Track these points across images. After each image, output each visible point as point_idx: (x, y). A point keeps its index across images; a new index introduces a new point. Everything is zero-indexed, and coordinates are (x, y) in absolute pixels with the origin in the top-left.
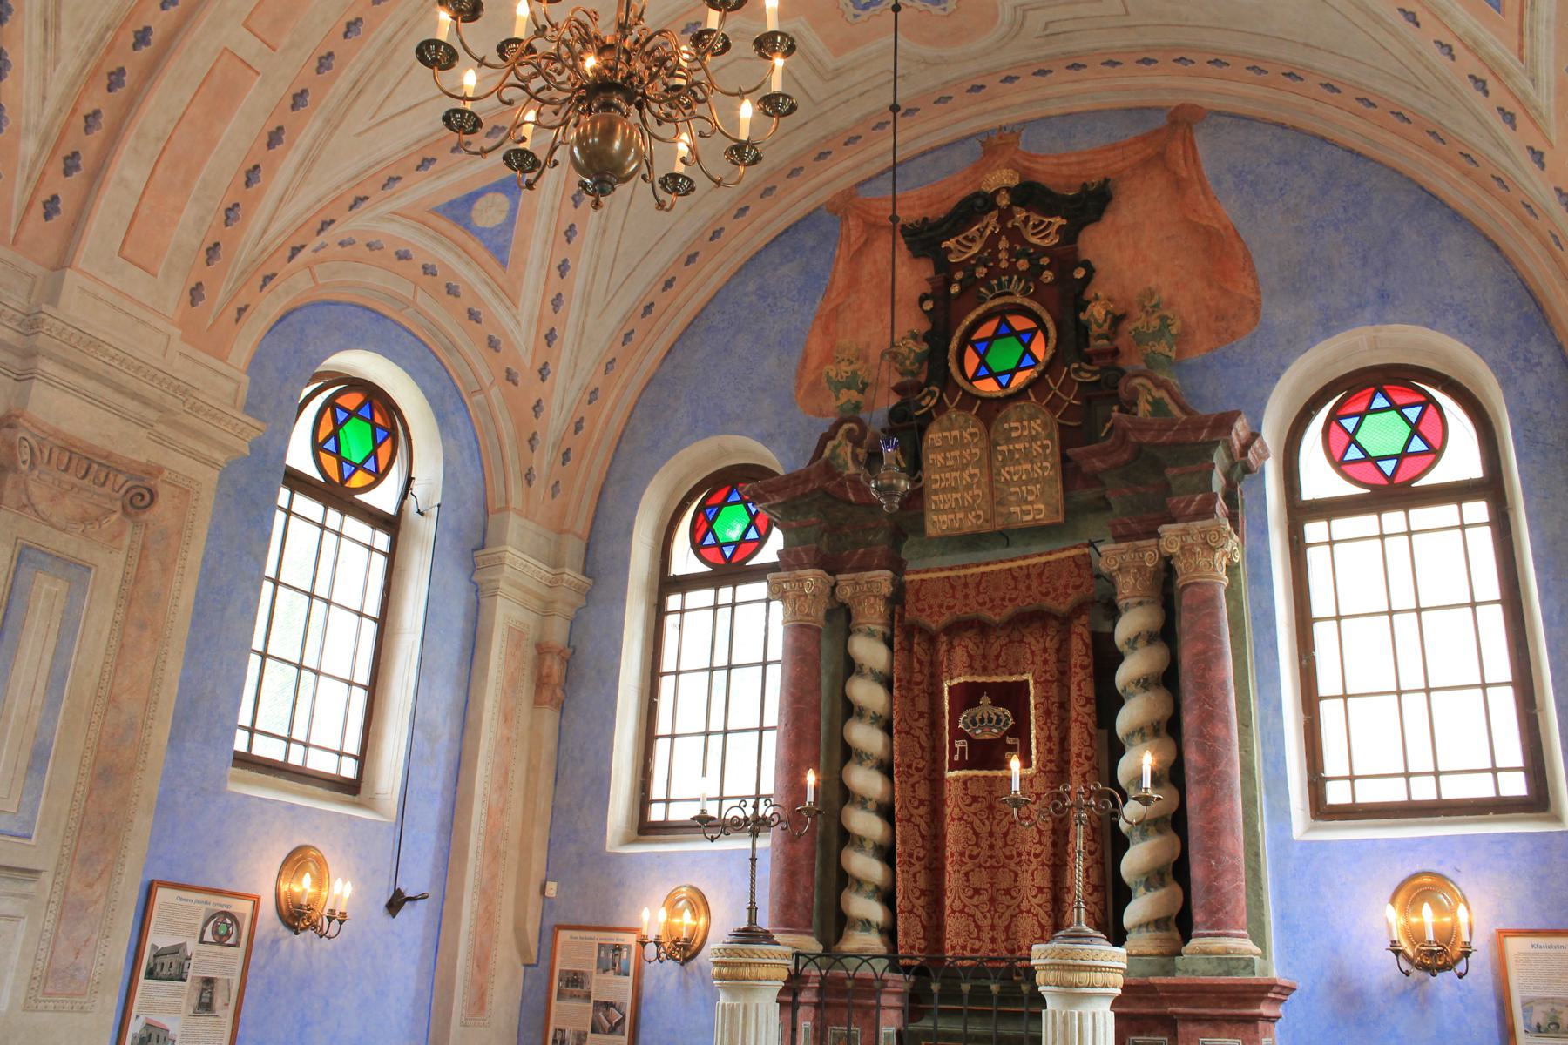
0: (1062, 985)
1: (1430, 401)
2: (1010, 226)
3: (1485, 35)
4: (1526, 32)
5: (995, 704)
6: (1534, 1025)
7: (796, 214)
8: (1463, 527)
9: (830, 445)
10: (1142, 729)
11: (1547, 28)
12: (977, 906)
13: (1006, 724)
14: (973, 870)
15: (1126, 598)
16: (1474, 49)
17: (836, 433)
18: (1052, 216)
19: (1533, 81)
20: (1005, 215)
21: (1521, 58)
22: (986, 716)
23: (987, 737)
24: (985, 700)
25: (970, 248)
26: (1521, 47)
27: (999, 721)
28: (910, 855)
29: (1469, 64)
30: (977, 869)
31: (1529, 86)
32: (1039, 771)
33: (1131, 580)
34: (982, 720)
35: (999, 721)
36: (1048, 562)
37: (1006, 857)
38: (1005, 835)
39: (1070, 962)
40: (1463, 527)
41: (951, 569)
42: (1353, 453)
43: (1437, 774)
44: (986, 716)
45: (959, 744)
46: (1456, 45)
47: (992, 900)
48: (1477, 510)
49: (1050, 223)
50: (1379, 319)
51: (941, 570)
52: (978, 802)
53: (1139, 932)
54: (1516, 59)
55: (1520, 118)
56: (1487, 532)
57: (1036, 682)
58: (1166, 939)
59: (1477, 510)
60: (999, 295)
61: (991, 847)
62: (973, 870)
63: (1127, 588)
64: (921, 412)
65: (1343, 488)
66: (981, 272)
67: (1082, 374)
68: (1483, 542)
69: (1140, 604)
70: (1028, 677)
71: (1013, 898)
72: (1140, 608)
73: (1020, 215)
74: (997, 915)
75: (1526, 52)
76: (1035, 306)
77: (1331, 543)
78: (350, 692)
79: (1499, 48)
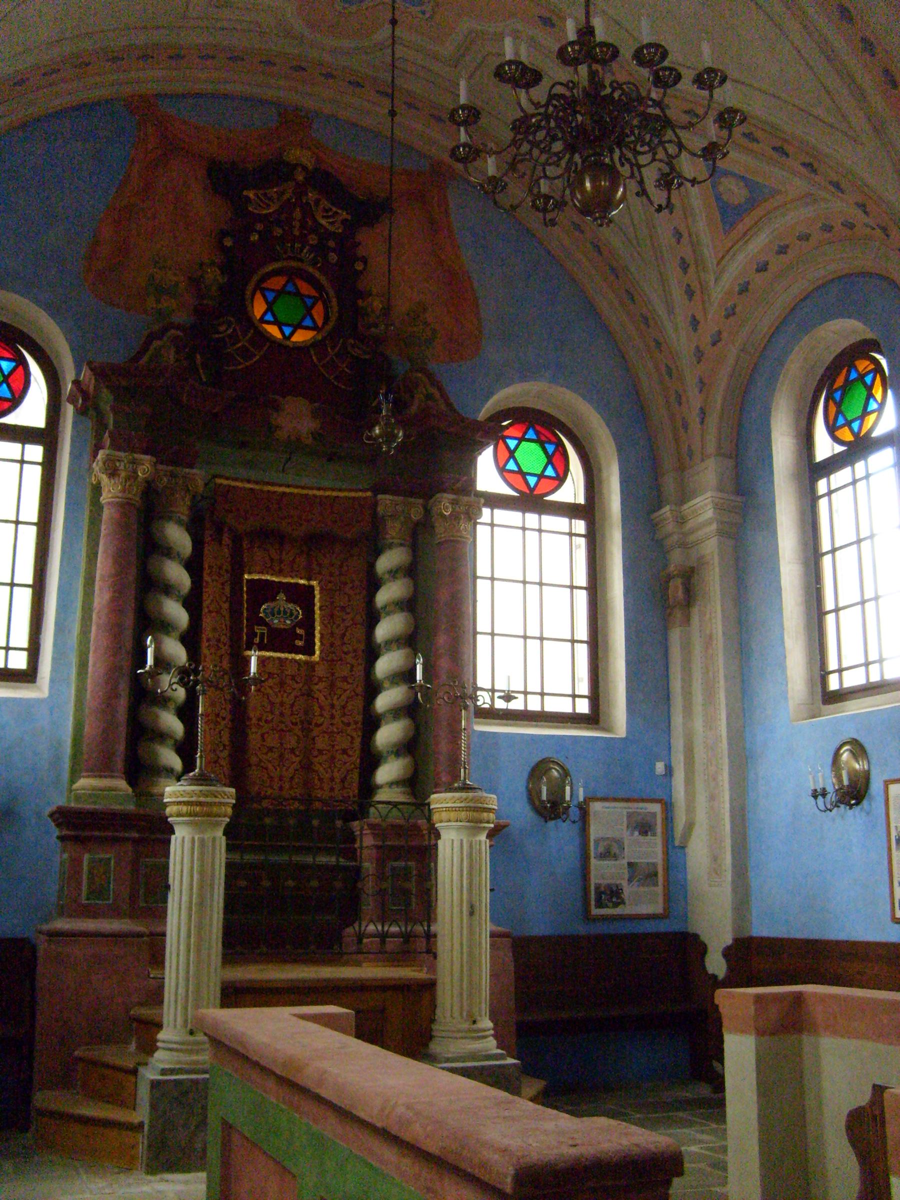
0: (472, 822)
1: (560, 446)
2: (304, 201)
3: (705, 239)
4: (731, 253)
5: (289, 600)
6: (599, 854)
7: (95, 94)
8: (22, 462)
9: (156, 344)
10: (398, 640)
11: (745, 257)
12: (270, 762)
13: (297, 617)
14: (268, 733)
15: (393, 538)
16: (695, 246)
17: (163, 335)
18: (341, 208)
19: (716, 280)
20: (300, 190)
21: (718, 264)
22: (282, 609)
23: (282, 627)
24: (281, 597)
25: (268, 206)
26: (723, 257)
27: (292, 614)
28: (218, 715)
29: (686, 250)
30: (271, 732)
31: (712, 283)
32: (321, 658)
33: (398, 525)
34: (279, 613)
35: (292, 614)
36: (338, 497)
37: (293, 724)
38: (344, 707)
39: (480, 805)
40: (22, 462)
41: (257, 483)
42: (511, 466)
43: (542, 694)
44: (282, 609)
45: (258, 630)
46: (686, 235)
47: (281, 756)
48: (35, 452)
49: (336, 213)
50: (554, 380)
51: (249, 481)
52: (273, 678)
53: (390, 787)
54: (715, 263)
55: (697, 297)
56: (38, 470)
57: (322, 590)
58: (401, 793)
59: (35, 452)
60: (290, 258)
61: (332, 717)
62: (268, 733)
63: (394, 530)
64: (217, 336)
65: (501, 488)
66: (278, 232)
67: (356, 349)
68: (34, 476)
69: (402, 545)
70: (314, 583)
71: (349, 756)
72: (402, 548)
73: (312, 195)
74: (285, 768)
75: (723, 263)
76: (323, 280)
77: (540, 531)
78: (857, 604)
79: (708, 253)
